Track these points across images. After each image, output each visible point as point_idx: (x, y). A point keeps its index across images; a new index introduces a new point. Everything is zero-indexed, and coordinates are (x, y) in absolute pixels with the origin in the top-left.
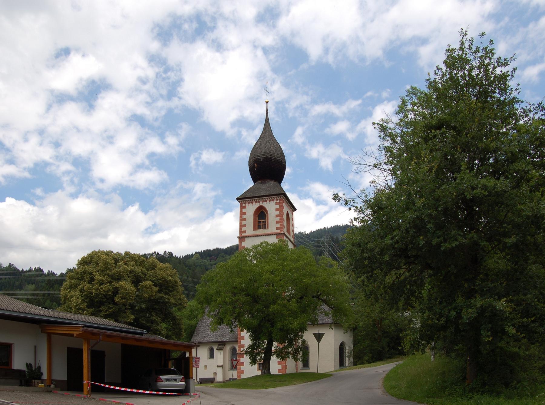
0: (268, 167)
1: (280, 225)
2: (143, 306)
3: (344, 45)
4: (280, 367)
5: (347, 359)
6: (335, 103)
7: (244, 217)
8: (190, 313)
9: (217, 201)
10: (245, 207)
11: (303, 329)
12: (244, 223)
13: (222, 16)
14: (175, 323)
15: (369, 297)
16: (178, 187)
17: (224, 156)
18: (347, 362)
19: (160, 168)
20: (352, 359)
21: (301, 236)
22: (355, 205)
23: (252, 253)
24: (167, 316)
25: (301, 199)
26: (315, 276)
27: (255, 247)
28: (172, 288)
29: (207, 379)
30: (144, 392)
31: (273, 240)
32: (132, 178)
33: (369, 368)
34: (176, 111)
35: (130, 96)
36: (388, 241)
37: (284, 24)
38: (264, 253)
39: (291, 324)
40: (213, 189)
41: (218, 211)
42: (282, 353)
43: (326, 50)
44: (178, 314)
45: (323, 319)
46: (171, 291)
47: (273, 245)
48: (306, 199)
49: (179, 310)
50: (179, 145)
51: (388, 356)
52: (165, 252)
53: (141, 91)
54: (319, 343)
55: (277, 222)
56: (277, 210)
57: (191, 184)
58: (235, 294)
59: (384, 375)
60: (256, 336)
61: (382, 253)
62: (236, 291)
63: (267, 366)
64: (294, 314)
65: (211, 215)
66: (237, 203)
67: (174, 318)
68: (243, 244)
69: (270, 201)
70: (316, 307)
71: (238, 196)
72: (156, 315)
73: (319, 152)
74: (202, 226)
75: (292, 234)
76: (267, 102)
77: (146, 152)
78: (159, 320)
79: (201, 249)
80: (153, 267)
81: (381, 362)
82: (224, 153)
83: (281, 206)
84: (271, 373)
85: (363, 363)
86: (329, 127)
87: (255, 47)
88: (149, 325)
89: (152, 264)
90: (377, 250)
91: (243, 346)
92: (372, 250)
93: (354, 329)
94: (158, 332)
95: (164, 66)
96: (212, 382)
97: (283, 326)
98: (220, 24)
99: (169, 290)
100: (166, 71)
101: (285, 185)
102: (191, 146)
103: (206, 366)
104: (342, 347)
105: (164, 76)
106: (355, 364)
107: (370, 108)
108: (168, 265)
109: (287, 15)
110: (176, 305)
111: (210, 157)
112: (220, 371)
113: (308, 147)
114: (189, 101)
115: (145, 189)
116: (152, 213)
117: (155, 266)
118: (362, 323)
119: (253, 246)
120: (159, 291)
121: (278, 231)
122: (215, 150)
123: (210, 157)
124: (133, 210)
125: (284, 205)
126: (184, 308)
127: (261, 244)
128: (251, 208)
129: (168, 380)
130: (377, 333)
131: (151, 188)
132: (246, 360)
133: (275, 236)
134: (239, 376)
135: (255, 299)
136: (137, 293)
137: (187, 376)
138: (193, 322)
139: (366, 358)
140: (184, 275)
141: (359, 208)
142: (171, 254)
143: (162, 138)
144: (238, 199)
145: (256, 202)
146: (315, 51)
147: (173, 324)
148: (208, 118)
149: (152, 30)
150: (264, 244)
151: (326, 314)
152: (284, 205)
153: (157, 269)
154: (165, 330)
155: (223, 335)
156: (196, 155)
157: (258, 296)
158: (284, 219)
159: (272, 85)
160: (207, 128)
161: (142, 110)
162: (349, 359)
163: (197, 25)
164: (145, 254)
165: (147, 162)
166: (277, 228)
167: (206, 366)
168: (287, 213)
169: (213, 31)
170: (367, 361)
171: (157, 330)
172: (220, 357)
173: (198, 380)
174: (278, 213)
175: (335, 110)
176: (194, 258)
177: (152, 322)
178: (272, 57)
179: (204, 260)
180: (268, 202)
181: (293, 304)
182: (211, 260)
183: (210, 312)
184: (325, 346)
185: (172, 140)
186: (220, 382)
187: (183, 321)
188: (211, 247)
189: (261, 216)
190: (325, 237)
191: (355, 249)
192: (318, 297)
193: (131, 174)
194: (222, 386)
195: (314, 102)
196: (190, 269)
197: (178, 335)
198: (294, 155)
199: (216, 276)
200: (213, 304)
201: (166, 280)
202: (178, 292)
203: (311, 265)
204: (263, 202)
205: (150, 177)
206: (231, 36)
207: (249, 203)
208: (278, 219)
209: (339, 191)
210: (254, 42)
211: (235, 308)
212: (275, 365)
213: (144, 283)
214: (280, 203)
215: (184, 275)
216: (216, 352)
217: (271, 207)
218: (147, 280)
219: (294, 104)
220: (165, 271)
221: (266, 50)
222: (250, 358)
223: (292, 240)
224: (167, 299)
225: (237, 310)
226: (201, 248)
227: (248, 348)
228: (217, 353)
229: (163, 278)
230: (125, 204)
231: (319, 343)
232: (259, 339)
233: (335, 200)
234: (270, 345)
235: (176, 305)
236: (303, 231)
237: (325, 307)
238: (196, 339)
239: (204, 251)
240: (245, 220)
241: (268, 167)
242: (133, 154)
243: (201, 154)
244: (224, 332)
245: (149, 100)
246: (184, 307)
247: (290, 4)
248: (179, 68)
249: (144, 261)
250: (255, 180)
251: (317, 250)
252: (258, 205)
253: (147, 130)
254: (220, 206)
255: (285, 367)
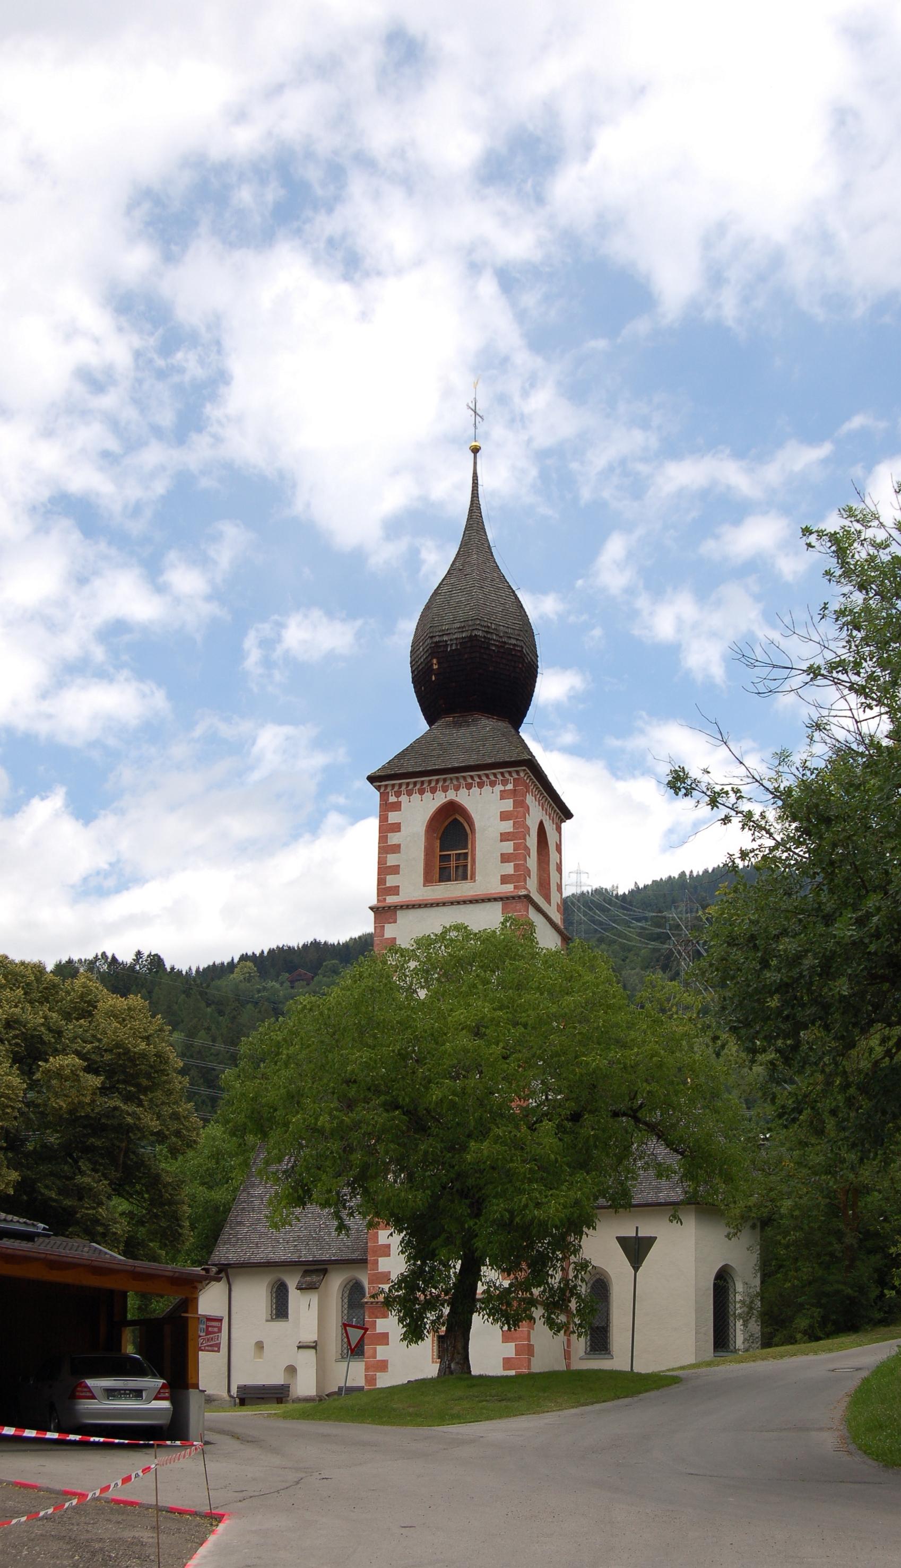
0: (475, 672)
1: (516, 867)
2: (53, 1139)
3: (777, 260)
4: (509, 1350)
5: (739, 1324)
6: (739, 454)
7: (394, 839)
8: (212, 1164)
9: (331, 780)
10: (397, 807)
11: (579, 1222)
12: (392, 860)
13: (366, 162)
14: (158, 1198)
15: (794, 1120)
16: (198, 732)
17: (359, 635)
18: (739, 1336)
19: (141, 675)
20: (755, 1327)
21: (600, 903)
22: (745, 806)
23: (413, 964)
24: (131, 1175)
25: (618, 778)
26: (623, 1045)
27: (425, 943)
28: (148, 1076)
29: (264, 1387)
30: (19, 1433)
31: (486, 919)
32: (46, 706)
33: (811, 1357)
34: (205, 483)
35: (48, 433)
36: (845, 930)
37: (571, 189)
38: (459, 962)
39: (538, 1205)
40: (319, 744)
41: (334, 818)
42: (509, 1304)
43: (715, 278)
44: (168, 1168)
45: (645, 1187)
46: (145, 1090)
47: (487, 938)
48: (634, 777)
49: (174, 1152)
50: (209, 598)
51: (878, 1316)
52: (139, 954)
53: (85, 414)
54: (636, 1269)
55: (505, 858)
56: (504, 816)
57: (246, 726)
58: (350, 1105)
59: (853, 1383)
60: (421, 1248)
61: (827, 969)
62: (352, 1092)
63: (460, 1346)
64: (548, 1174)
65: (312, 826)
66: (373, 794)
67: (155, 1181)
68: (390, 931)
69: (481, 785)
70: (627, 1148)
71: (373, 769)
72: (95, 1170)
73: (679, 620)
74: (259, 872)
75: (555, 898)
76: (475, 450)
77: (98, 621)
78: (103, 1186)
79: (260, 944)
80: (85, 1009)
81: (854, 1337)
82: (359, 623)
83: (520, 804)
84: (475, 1371)
85: (792, 1340)
86: (717, 537)
87: (474, 268)
88: (68, 1202)
89: (82, 997)
90: (809, 961)
91: (385, 1277)
92: (795, 961)
93: (764, 1223)
94: (100, 1229)
95: (161, 331)
96: (280, 1401)
97: (511, 1212)
98: (357, 185)
99: (138, 1085)
100: (169, 344)
101: (530, 736)
102: (248, 601)
103: (260, 1346)
104: (722, 1282)
105: (160, 363)
106: (767, 1342)
107: (858, 471)
108: (136, 1000)
109: (585, 160)
110: (161, 1137)
111: (311, 636)
112: (307, 1364)
113: (642, 602)
114: (245, 448)
115: (92, 745)
116: (107, 822)
117: (93, 1004)
118: (788, 1203)
119: (418, 942)
120: (104, 1090)
121: (509, 888)
122: (330, 614)
123: (311, 636)
124: (45, 810)
125: (530, 800)
126: (189, 1146)
127: (446, 931)
128: (418, 810)
129: (111, 1393)
130: (839, 1235)
131: (111, 742)
132: (390, 1325)
133: (499, 905)
134: (371, 1380)
135: (418, 1121)
136: (31, 1095)
137: (179, 1380)
138: (219, 1195)
139: (802, 1323)
140: (202, 1033)
141: (756, 817)
142: (156, 961)
143: (153, 573)
144: (372, 779)
145: (433, 791)
146: (675, 281)
147: (152, 1202)
148: (308, 505)
149: (130, 208)
150: (453, 934)
151: (662, 1172)
152: (530, 800)
153: (99, 1016)
154: (124, 1221)
155: (319, 1240)
156: (266, 628)
157: (428, 1111)
158: (527, 849)
159: (525, 394)
160: (308, 538)
161: (86, 479)
162: (745, 1325)
163: (282, 192)
164: (70, 962)
165: (99, 654)
166: (505, 879)
167: (260, 1346)
168: (541, 825)
169: (330, 210)
170: (805, 1333)
171: (96, 1221)
172: (310, 1313)
173: (234, 1391)
174: (508, 826)
175: (734, 475)
176: (236, 975)
177: (81, 1193)
178: (530, 299)
179: (271, 984)
180: (475, 790)
181: (547, 1140)
182: (292, 982)
183: (267, 1163)
184: (666, 1280)
185: (187, 580)
186: (307, 1400)
187: (187, 1190)
188: (296, 940)
189: (451, 836)
190: (682, 907)
191: (738, 955)
192: (634, 1114)
193: (44, 695)
194: (305, 1415)
195: (672, 450)
196: (221, 1013)
197: (171, 1238)
198: (597, 632)
199: (288, 1042)
200: (275, 1135)
201: (127, 1051)
202: (169, 1093)
203: (609, 1007)
204: (457, 789)
205: (106, 704)
206: (392, 228)
207: (410, 793)
208: (508, 847)
209: (746, 752)
210: (471, 251)
211: (349, 1149)
212: (489, 1349)
213: (55, 1062)
214: (514, 792)
215: (202, 1033)
216: (294, 1295)
217: (486, 806)
218: (64, 1052)
219: (599, 459)
220: (126, 1021)
221: (509, 280)
222: (401, 1320)
223: (557, 918)
224: (133, 1115)
225: (357, 1157)
226: (261, 942)
227: (398, 1285)
228: (298, 1302)
229: (118, 1046)
230: (21, 792)
231: (636, 1269)
232: (432, 1256)
233: (676, 790)
234: (471, 1273)
235: (161, 1137)
236: (607, 885)
237: (661, 1151)
238: (225, 1253)
239: (271, 952)
240: (396, 849)
241: (475, 672)
242: (52, 627)
243: (281, 625)
244: (312, 1230)
245: (113, 445)
246: (191, 1144)
247: (592, 120)
248: (210, 340)
249: (55, 986)
250: (431, 716)
251: (655, 950)
252: (441, 799)
253: (103, 546)
254: (342, 800)
255: (528, 1350)
